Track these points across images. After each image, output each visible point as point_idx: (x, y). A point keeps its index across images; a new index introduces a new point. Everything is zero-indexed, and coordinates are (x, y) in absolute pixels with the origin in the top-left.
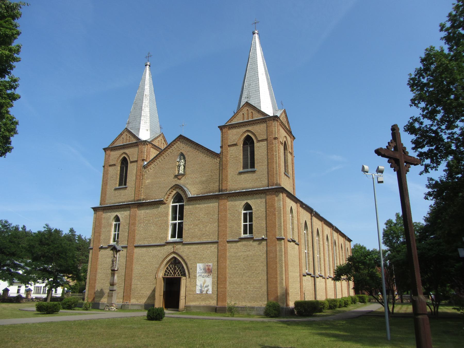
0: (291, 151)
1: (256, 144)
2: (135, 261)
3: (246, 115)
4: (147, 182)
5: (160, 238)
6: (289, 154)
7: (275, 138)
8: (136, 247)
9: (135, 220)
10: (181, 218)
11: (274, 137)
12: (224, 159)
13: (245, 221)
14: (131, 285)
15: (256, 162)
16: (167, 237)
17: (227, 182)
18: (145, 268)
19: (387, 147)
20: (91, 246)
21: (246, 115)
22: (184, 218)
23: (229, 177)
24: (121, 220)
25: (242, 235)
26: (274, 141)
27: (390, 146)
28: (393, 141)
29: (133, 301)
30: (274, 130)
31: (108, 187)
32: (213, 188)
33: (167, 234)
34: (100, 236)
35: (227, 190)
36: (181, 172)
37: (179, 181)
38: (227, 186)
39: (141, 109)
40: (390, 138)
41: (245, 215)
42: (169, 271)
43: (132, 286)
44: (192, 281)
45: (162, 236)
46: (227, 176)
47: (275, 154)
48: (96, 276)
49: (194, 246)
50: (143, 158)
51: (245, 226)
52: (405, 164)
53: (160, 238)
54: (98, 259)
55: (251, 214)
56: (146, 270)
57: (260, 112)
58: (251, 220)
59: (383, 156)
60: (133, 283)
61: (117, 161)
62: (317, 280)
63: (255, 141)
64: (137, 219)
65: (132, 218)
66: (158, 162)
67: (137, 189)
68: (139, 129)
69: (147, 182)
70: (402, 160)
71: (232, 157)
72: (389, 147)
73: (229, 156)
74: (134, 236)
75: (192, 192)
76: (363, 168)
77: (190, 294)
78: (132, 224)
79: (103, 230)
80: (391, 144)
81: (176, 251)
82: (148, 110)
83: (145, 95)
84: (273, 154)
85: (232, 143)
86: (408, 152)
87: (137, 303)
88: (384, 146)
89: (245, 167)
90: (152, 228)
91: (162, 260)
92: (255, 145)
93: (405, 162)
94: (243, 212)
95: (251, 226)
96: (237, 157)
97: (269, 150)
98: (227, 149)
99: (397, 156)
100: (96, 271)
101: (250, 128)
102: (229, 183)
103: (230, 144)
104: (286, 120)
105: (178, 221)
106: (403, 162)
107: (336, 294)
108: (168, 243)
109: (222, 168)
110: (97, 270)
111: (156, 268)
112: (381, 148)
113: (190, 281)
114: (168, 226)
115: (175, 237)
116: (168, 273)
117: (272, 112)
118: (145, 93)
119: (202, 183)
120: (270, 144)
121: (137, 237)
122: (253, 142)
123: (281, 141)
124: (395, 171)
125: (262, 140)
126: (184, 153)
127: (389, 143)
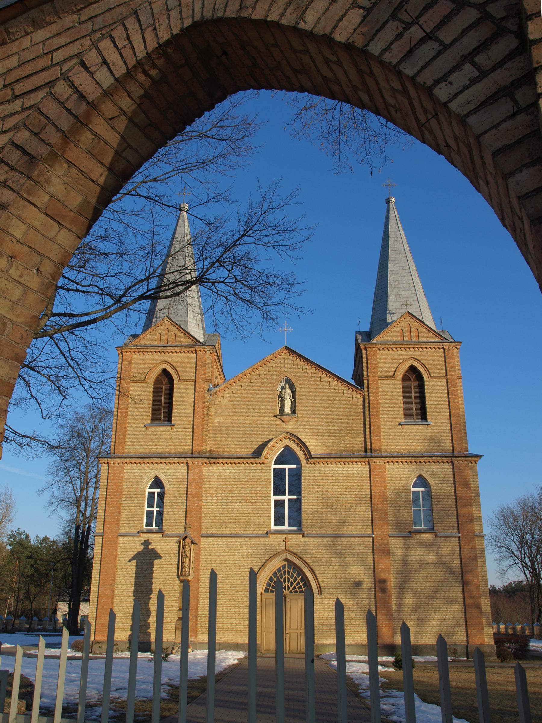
4: (217, 420)
5: (254, 524)
13: (150, 505)
17: (380, 437)
18: (227, 578)
23: (383, 429)
24: (167, 486)
25: (145, 527)
31: (129, 420)
35: (380, 450)
37: (284, 425)
41: (151, 495)
43: (200, 609)
45: (259, 520)
46: (379, 427)
48: (113, 590)
49: (249, 532)
51: (150, 514)
54: (116, 556)
55: (161, 496)
56: (227, 581)
58: (161, 504)
60: (200, 605)
63: (425, 376)
64: (205, 486)
66: (239, 388)
69: (217, 420)
71: (386, 397)
78: (195, 496)
79: (125, 501)
85: (385, 375)
89: (408, 415)
90: (238, 506)
92: (426, 383)
94: (148, 490)
95: (160, 514)
96: (395, 398)
98: (377, 383)
100: (114, 580)
101: (167, 357)
103: (380, 375)
105: (286, 498)
109: (368, 412)
115: (283, 525)
120: (453, 385)
121: (205, 521)
122: (171, 381)
126: (293, 380)
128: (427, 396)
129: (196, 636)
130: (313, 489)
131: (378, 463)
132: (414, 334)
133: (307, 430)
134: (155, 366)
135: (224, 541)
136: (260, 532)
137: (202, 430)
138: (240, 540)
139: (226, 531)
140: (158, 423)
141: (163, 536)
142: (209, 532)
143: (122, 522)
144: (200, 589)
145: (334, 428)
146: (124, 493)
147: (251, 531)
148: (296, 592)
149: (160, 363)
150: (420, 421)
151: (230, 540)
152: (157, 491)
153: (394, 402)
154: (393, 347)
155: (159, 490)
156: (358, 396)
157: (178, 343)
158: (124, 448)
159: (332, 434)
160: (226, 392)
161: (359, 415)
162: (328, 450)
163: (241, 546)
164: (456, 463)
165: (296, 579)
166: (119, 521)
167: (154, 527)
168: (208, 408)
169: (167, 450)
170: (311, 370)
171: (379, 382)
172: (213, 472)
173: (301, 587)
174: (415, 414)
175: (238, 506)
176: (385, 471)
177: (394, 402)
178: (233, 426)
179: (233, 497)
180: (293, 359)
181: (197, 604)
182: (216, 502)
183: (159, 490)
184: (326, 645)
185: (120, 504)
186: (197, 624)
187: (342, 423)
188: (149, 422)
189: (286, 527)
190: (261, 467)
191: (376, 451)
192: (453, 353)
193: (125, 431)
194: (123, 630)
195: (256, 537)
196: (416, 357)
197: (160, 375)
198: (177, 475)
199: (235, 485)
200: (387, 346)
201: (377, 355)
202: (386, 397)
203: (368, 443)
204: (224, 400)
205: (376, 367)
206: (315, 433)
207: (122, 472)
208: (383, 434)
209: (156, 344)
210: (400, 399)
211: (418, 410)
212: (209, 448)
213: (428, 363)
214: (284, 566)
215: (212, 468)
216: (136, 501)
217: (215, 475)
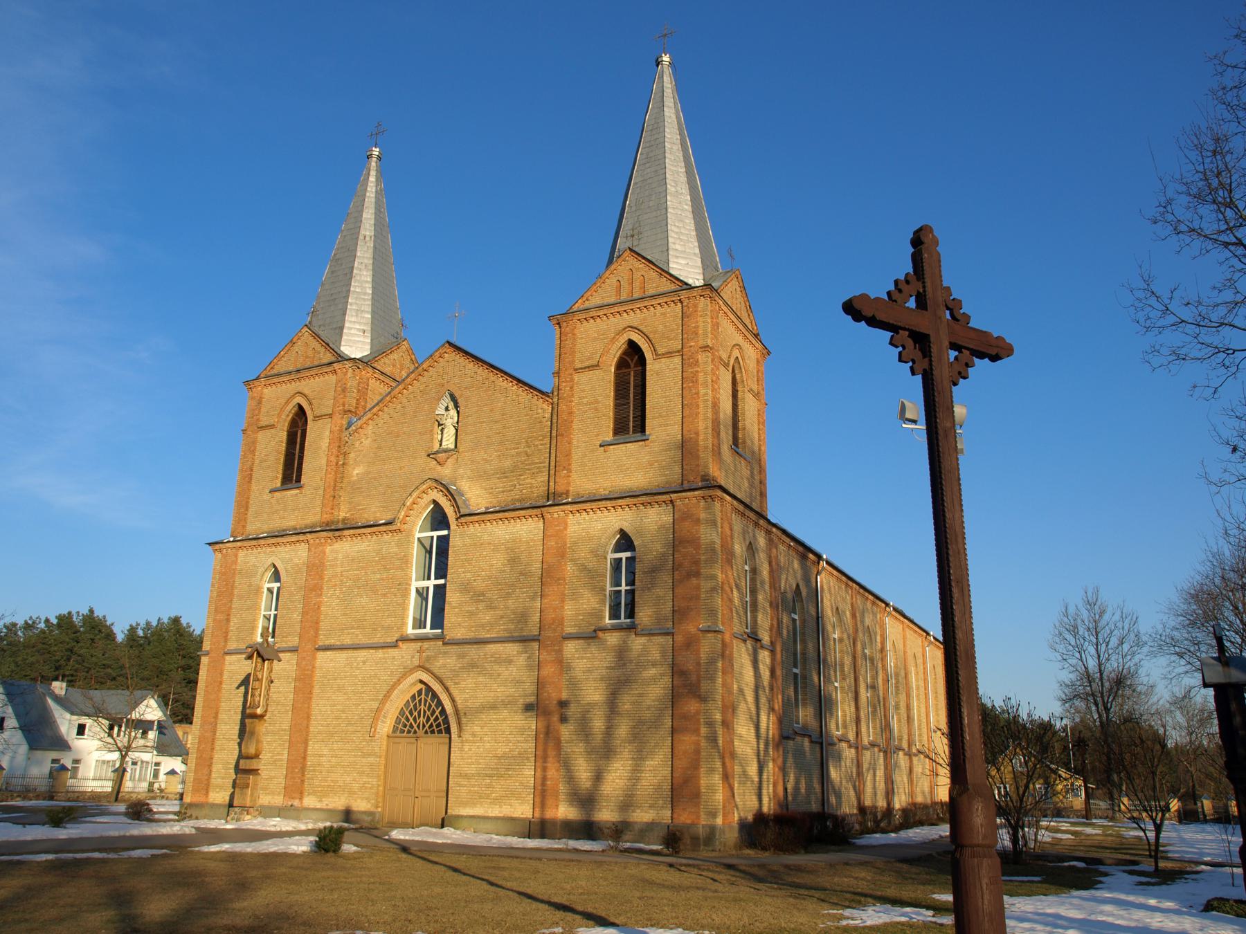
0: (755, 388)
1: (652, 366)
2: (316, 690)
3: (625, 284)
4: (356, 472)
5: (383, 628)
6: (749, 397)
7: (705, 348)
8: (318, 649)
9: (322, 579)
10: (442, 572)
11: (701, 343)
12: (562, 407)
14: (305, 758)
15: (648, 416)
16: (404, 624)
17: (569, 471)
19: (889, 293)
20: (206, 646)
21: (625, 284)
22: (450, 571)
23: (576, 456)
25: (607, 621)
26: (701, 357)
27: (900, 291)
28: (913, 279)
29: (309, 801)
30: (701, 324)
31: (254, 486)
32: (535, 485)
33: (403, 617)
34: (228, 620)
36: (449, 442)
37: (439, 468)
38: (569, 483)
39: (349, 275)
40: (906, 267)
42: (408, 720)
44: (466, 747)
45: (389, 621)
46: (569, 455)
47: (702, 391)
48: (214, 732)
49: (376, 640)
50: (347, 407)
52: (953, 354)
53: (383, 628)
54: (221, 683)
56: (344, 716)
57: (664, 272)
59: (873, 322)
61: (279, 415)
62: (915, 759)
63: (648, 356)
64: (328, 573)
65: (316, 569)
67: (333, 493)
68: (342, 328)
69: (356, 472)
70: (940, 341)
71: (585, 401)
72: (896, 296)
73: (576, 399)
74: (317, 623)
75: (476, 496)
76: (903, 409)
77: (460, 785)
80: (903, 286)
81: (427, 665)
82: (369, 279)
83: (361, 237)
84: (697, 393)
85: (587, 364)
86: (967, 317)
87: (319, 806)
88: (879, 288)
91: (386, 688)
92: (648, 367)
93: (954, 346)
96: (597, 402)
97: (687, 380)
98: (572, 380)
99: (922, 323)
100: (216, 717)
101: (631, 319)
102: (574, 476)
103: (579, 366)
104: (740, 299)
106: (946, 343)
107: (889, 793)
108: (405, 639)
109: (557, 430)
110: (217, 713)
111: (371, 710)
112: (864, 297)
113: (461, 750)
114: (406, 594)
116: (405, 726)
117: (701, 277)
118: (362, 232)
119: (503, 474)
120: (690, 365)
122: (642, 361)
123: (725, 356)
124: (913, 373)
125: (669, 354)
127: (896, 282)
128: (648, 390)
129: (301, 799)
130: (462, 567)
131: (556, 515)
132: (637, 284)
133: (469, 473)
134: (287, 402)
135: (343, 655)
136: (389, 640)
137: (334, 490)
138: (363, 654)
139: (347, 641)
140: (290, 486)
141: (444, 644)
142: (327, 643)
143: (231, 634)
144: (312, 729)
145: (507, 463)
146: (236, 592)
147: (378, 638)
148: (433, 732)
149: (293, 396)
150: (638, 436)
151: (351, 653)
152: (624, 555)
153: (596, 409)
154: (601, 313)
155: (628, 554)
156: (545, 406)
157: (650, 292)
158: (244, 527)
159: (503, 474)
160: (370, 429)
161: (544, 437)
162: (495, 501)
163: (364, 662)
164: (678, 503)
165: (434, 712)
166: (227, 633)
167: (623, 620)
168: (345, 454)
169: (293, 523)
170: (482, 372)
171: (576, 377)
172: (341, 550)
173: (439, 725)
174: (631, 424)
175: (365, 600)
176: (565, 529)
177: (596, 409)
178: (375, 478)
179: (359, 588)
180: (460, 359)
181: (306, 750)
182: (338, 598)
183: (628, 554)
184: (462, 816)
185: (230, 608)
186: (303, 781)
187: (518, 454)
188: (279, 484)
189: (428, 630)
190: (397, 537)
191: (560, 495)
192: (696, 306)
193: (247, 502)
194: (221, 788)
195: (382, 647)
196: (635, 325)
197: (625, 353)
198: (296, 561)
199: (363, 568)
200: (592, 314)
201: (576, 331)
202: (585, 401)
203: (552, 484)
204: (365, 440)
205: (573, 353)
206: (480, 476)
207: (235, 563)
208: (574, 466)
209: (613, 300)
210: (609, 401)
211: (631, 417)
212: (342, 515)
213: (656, 332)
214: (420, 692)
215: (338, 546)
216: (249, 602)
217: (340, 557)
